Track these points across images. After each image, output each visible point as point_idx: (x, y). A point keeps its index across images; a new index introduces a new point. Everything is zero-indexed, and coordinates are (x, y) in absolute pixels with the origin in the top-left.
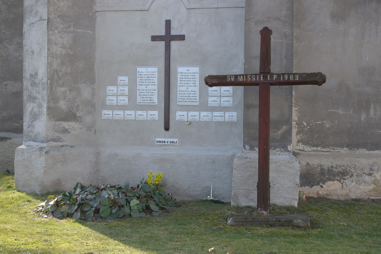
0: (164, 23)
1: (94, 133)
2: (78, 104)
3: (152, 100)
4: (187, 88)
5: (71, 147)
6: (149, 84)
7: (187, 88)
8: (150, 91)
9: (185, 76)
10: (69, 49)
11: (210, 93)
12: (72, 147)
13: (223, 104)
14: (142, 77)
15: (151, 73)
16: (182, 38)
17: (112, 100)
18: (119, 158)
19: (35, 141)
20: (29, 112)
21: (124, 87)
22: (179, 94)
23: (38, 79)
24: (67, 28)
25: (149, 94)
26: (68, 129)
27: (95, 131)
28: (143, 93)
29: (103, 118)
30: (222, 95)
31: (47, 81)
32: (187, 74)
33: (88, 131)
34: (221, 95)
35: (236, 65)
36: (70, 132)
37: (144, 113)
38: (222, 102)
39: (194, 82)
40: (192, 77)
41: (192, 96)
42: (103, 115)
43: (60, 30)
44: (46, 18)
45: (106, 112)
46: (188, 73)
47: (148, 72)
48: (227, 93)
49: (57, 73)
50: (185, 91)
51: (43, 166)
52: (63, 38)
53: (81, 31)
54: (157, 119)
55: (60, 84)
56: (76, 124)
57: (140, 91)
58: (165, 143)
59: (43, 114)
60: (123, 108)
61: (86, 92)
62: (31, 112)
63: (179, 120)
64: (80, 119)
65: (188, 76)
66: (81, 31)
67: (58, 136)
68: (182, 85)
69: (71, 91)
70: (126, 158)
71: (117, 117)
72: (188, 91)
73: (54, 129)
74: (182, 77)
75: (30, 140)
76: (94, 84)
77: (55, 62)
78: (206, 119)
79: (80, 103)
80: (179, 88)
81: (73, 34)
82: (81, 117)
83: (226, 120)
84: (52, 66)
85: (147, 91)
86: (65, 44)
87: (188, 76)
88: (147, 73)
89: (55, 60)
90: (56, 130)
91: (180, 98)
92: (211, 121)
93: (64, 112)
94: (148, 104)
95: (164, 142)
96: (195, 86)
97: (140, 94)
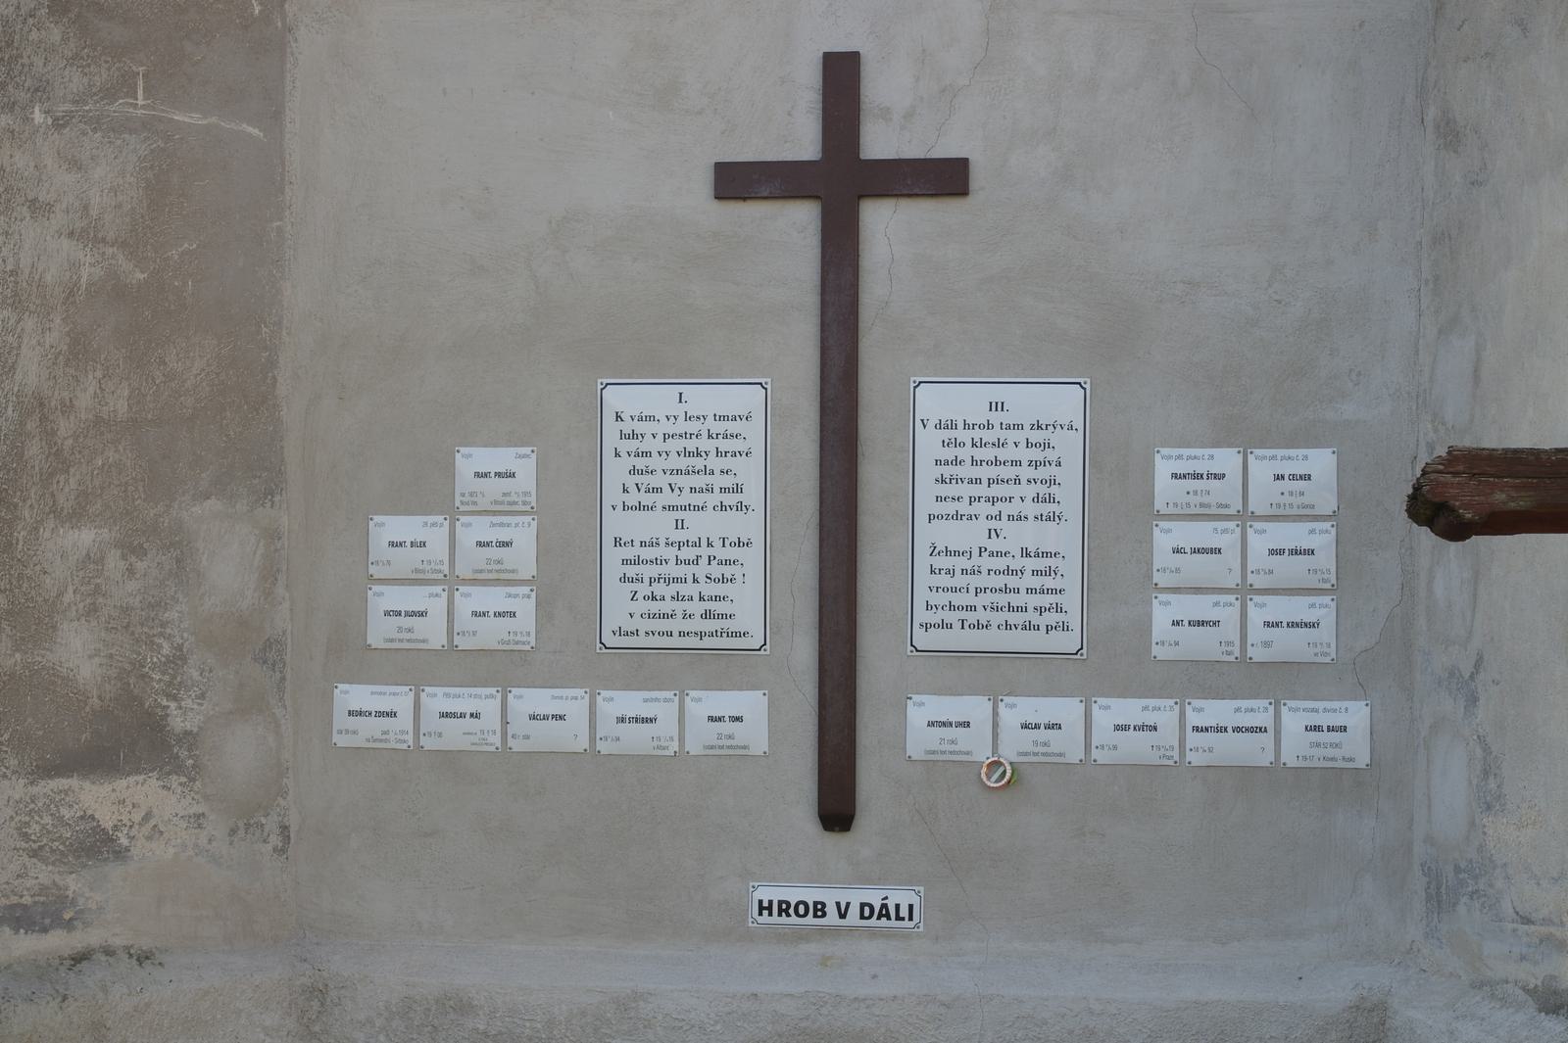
1: (275, 850)
2: (180, 648)
3: (722, 616)
5: (134, 961)
6: (697, 499)
8: (704, 551)
9: (974, 445)
10: (124, 245)
11: (1258, 572)
12: (143, 958)
13: (1267, 644)
14: (647, 454)
15: (719, 427)
16: (946, 178)
17: (412, 614)
18: (482, 1027)
22: (932, 572)
24: (109, 94)
25: (701, 570)
26: (116, 828)
27: (284, 829)
28: (655, 561)
29: (340, 741)
30: (1258, 581)
32: (988, 436)
33: (241, 833)
34: (1251, 579)
35: (1359, 374)
36: (127, 849)
37: (661, 706)
39: (1043, 490)
40: (1026, 455)
41: (1030, 591)
42: (340, 720)
43: (62, 108)
45: (354, 695)
46: (997, 426)
47: (688, 418)
48: (1293, 570)
49: (43, 419)
50: (976, 552)
52: (80, 169)
53: (194, 119)
54: (759, 744)
55: (61, 500)
56: (164, 787)
57: (629, 553)
58: (824, 915)
60: (499, 668)
61: (227, 563)
63: (934, 752)
64: (189, 750)
65: (1000, 444)
66: (194, 119)
67: (47, 888)
68: (950, 508)
69: (131, 549)
70: (528, 1024)
71: (454, 736)
72: (999, 554)
73: (26, 837)
74: (949, 453)
76: (277, 498)
77: (34, 342)
78: (1136, 748)
79: (192, 639)
80: (927, 534)
81: (147, 139)
82: (197, 734)
83: (1289, 758)
84: (13, 368)
85: (688, 553)
86: (94, 213)
87: (1000, 444)
88: (682, 426)
89: (29, 323)
90: (35, 846)
91: (942, 599)
92: (1171, 762)
93: (88, 709)
94: (692, 642)
95: (816, 910)
97: (631, 571)
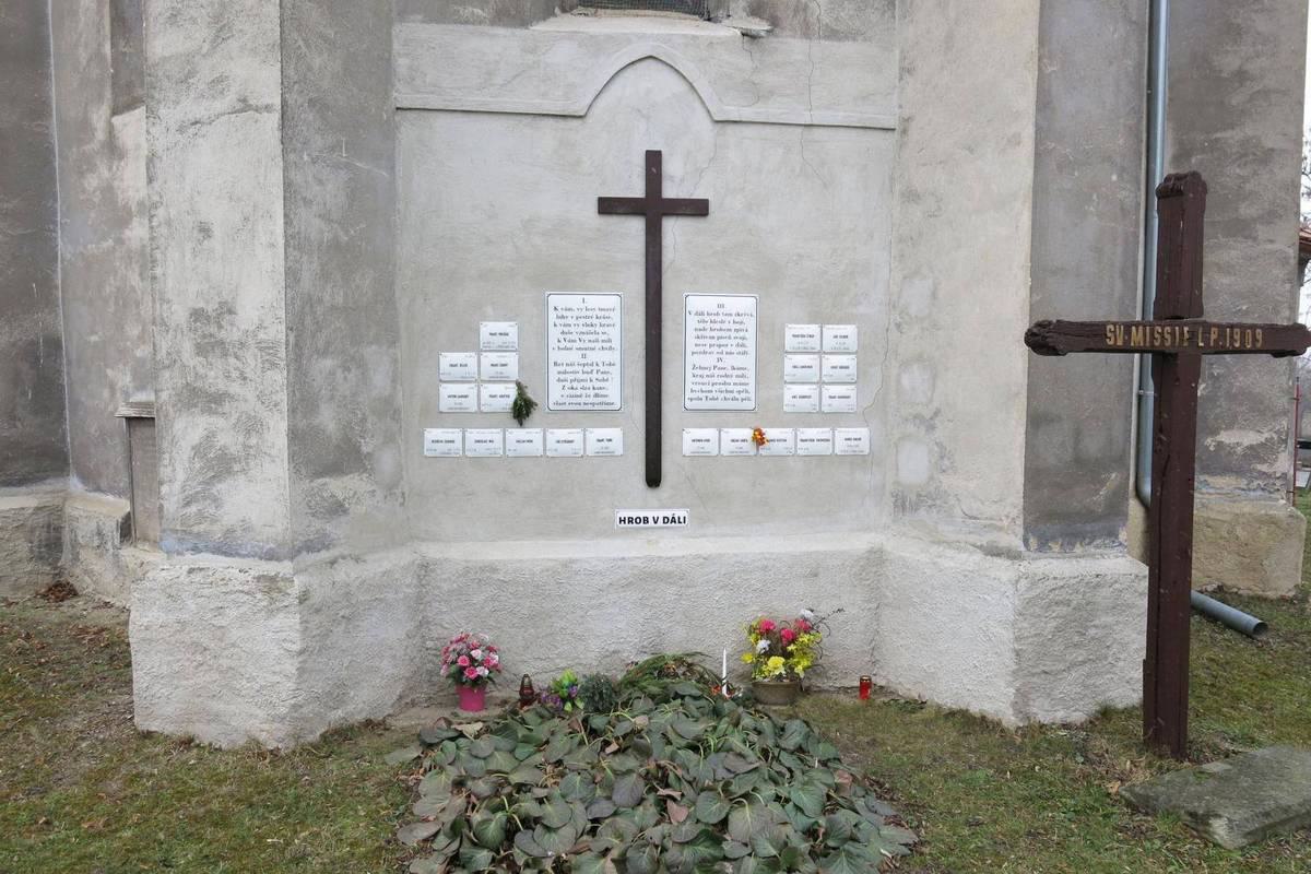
0: (640, 161)
3: (602, 396)
4: (719, 360)
7: (719, 360)
10: (340, 223)
15: (600, 314)
16: (699, 209)
19: (225, 549)
20: (189, 448)
21: (504, 354)
23: (239, 329)
24: (332, 149)
25: (594, 376)
26: (344, 500)
31: (287, 336)
32: (718, 319)
38: (826, 401)
39: (740, 342)
44: (277, 101)
45: (432, 434)
49: (311, 306)
51: (296, 647)
59: (269, 455)
62: (199, 451)
65: (722, 322)
73: (310, 507)
75: (196, 550)
83: (837, 451)
85: (587, 369)
87: (722, 322)
88: (584, 313)
96: (745, 353)
97: (562, 377)
